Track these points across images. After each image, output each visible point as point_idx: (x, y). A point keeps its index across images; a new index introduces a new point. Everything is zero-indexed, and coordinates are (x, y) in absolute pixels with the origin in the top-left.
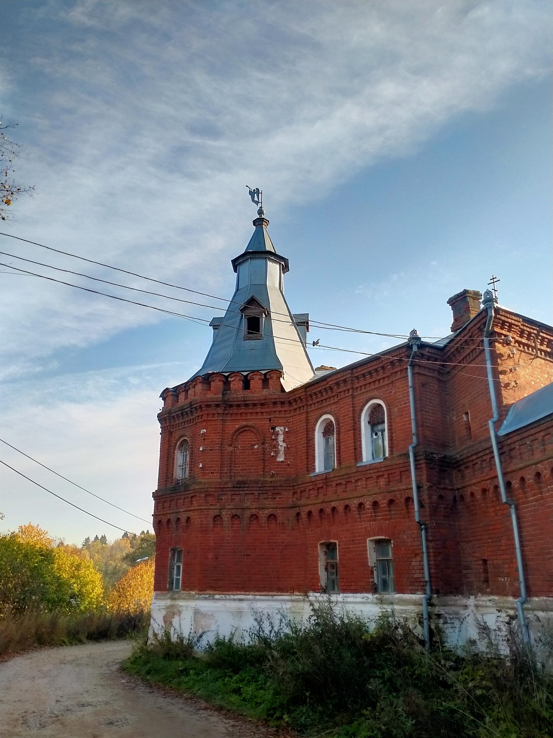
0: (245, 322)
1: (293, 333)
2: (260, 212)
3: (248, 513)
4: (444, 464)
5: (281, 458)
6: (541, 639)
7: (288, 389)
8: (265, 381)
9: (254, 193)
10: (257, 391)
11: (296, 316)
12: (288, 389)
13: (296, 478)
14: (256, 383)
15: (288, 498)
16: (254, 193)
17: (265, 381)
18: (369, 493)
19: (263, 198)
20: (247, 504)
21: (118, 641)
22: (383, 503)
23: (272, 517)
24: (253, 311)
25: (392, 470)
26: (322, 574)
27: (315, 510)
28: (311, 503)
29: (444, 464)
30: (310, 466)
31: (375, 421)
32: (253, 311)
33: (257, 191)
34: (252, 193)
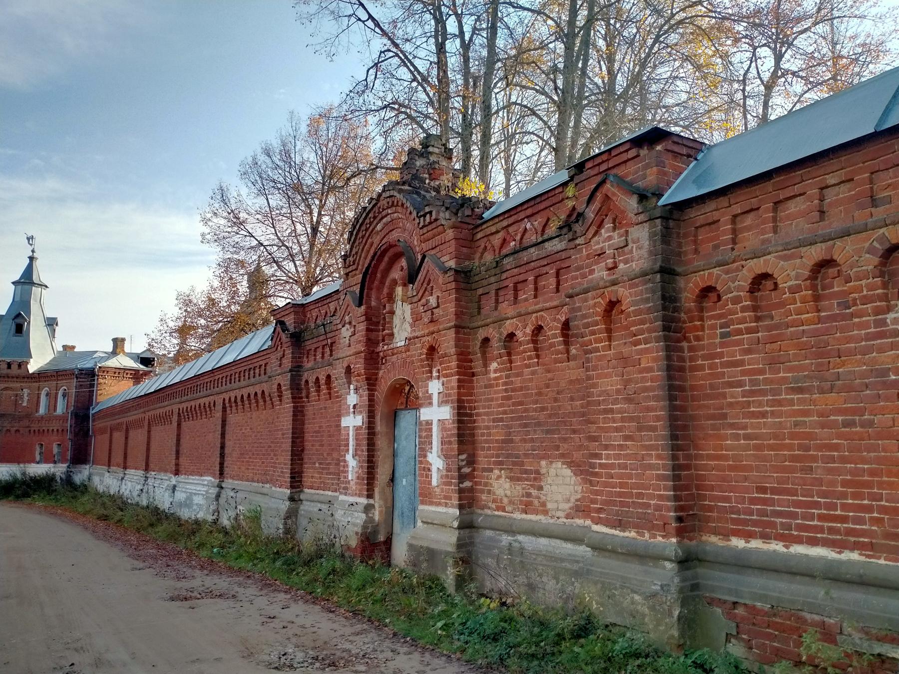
0: (14, 327)
1: (45, 331)
2: (33, 251)
3: (5, 429)
4: (82, 415)
5: (25, 404)
6: (772, 287)
7: (31, 371)
8: (20, 366)
9: (30, 239)
10: (15, 370)
11: (48, 318)
12: (31, 371)
13: (29, 415)
14: (14, 367)
15: (26, 422)
16: (30, 239)
17: (20, 366)
18: (55, 426)
19: (37, 242)
20: (5, 424)
21: (13, 505)
22: (60, 430)
23: (17, 431)
24: (19, 321)
25: (63, 418)
26: (38, 458)
27: (37, 429)
28: (35, 427)
29: (82, 415)
30: (37, 410)
31: (64, 395)
32: (19, 321)
33: (32, 237)
34: (28, 239)
